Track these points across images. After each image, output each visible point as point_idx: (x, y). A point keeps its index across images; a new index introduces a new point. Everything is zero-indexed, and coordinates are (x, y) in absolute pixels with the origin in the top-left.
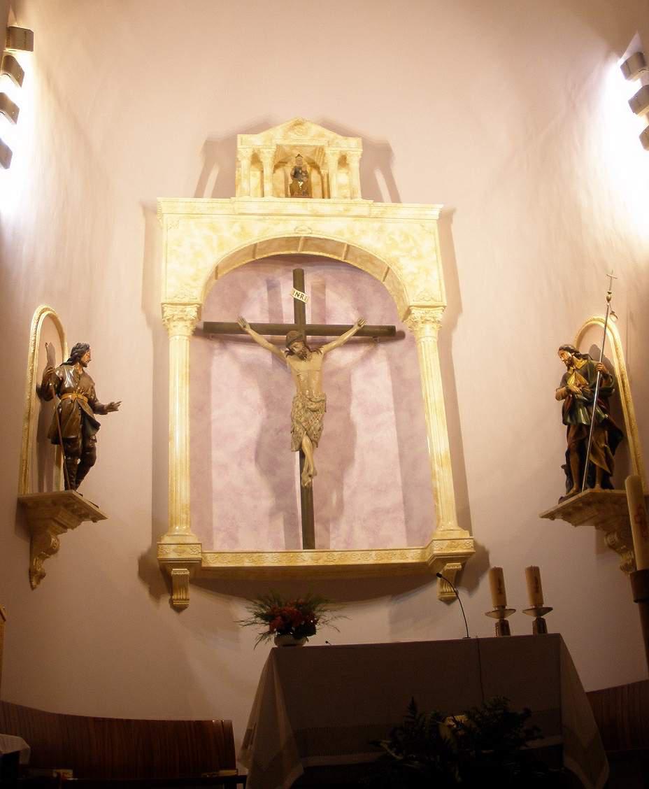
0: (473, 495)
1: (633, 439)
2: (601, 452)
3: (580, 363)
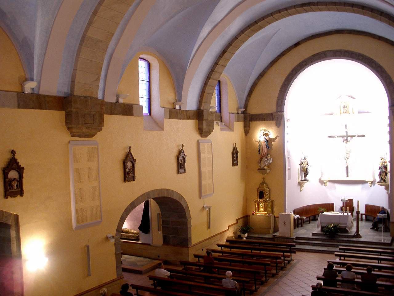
2: (384, 176)
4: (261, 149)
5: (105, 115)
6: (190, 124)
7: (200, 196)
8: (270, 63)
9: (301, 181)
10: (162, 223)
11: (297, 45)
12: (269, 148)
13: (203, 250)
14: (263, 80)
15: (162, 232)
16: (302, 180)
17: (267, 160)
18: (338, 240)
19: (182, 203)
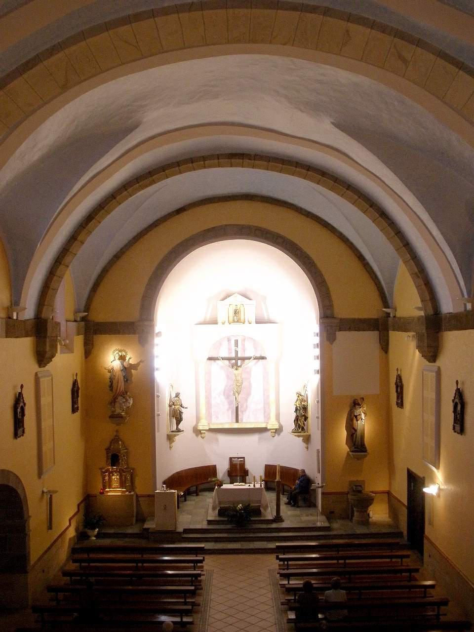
0: (282, 410)
1: (309, 420)
2: (302, 422)
3: (300, 397)
4: (115, 382)
7: (40, 474)
11: (180, 211)
12: (127, 380)
13: (43, 571)
16: (172, 432)
19: (20, 491)
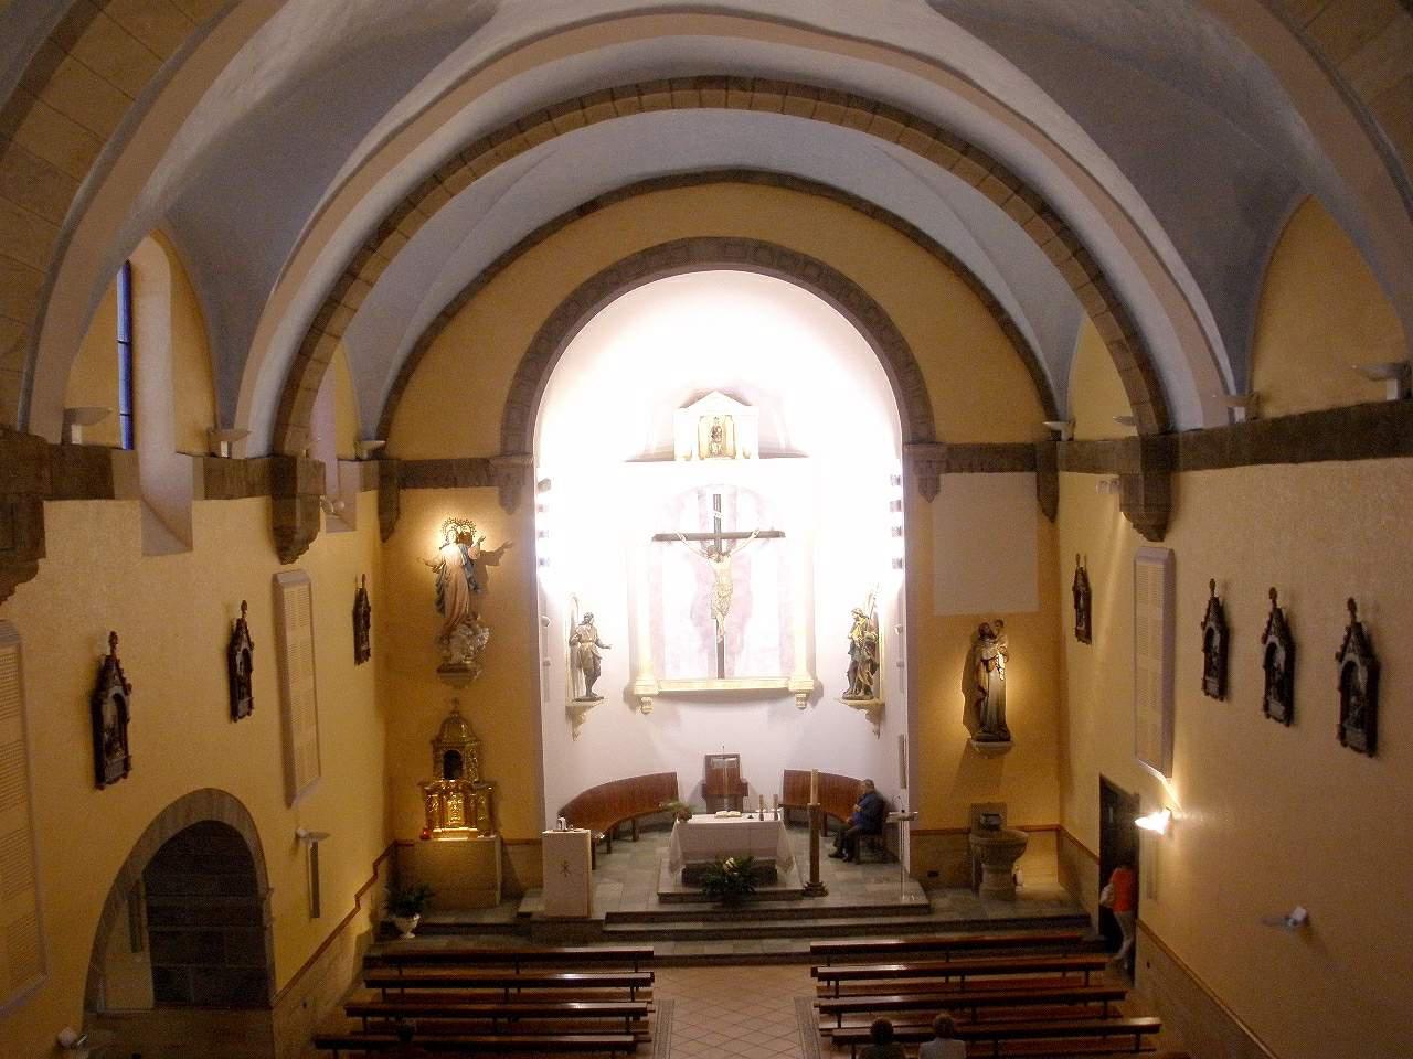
3: (862, 621)
5: (46, 504)
6: (248, 514)
8: (485, 272)
9: (575, 703)
10: (150, 918)
11: (587, 208)
14: (451, 331)
15: (148, 954)
16: (579, 700)
17: (471, 633)
18: (758, 911)
19: (247, 835)
